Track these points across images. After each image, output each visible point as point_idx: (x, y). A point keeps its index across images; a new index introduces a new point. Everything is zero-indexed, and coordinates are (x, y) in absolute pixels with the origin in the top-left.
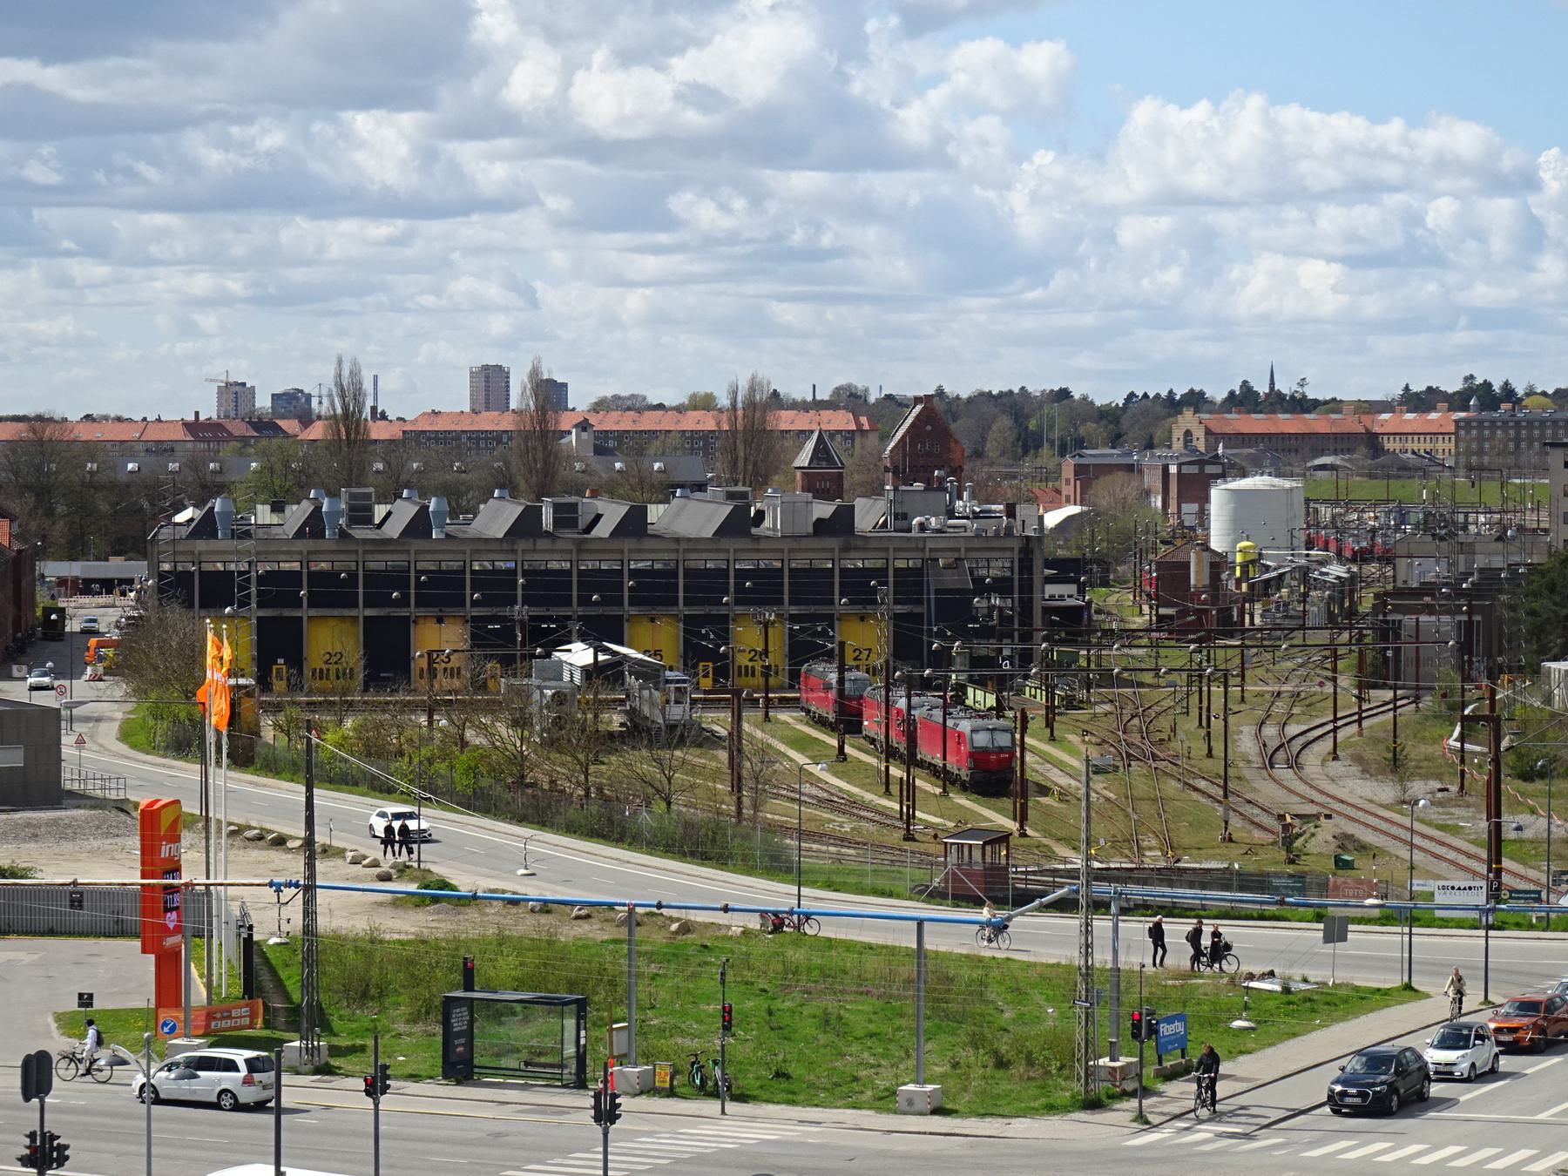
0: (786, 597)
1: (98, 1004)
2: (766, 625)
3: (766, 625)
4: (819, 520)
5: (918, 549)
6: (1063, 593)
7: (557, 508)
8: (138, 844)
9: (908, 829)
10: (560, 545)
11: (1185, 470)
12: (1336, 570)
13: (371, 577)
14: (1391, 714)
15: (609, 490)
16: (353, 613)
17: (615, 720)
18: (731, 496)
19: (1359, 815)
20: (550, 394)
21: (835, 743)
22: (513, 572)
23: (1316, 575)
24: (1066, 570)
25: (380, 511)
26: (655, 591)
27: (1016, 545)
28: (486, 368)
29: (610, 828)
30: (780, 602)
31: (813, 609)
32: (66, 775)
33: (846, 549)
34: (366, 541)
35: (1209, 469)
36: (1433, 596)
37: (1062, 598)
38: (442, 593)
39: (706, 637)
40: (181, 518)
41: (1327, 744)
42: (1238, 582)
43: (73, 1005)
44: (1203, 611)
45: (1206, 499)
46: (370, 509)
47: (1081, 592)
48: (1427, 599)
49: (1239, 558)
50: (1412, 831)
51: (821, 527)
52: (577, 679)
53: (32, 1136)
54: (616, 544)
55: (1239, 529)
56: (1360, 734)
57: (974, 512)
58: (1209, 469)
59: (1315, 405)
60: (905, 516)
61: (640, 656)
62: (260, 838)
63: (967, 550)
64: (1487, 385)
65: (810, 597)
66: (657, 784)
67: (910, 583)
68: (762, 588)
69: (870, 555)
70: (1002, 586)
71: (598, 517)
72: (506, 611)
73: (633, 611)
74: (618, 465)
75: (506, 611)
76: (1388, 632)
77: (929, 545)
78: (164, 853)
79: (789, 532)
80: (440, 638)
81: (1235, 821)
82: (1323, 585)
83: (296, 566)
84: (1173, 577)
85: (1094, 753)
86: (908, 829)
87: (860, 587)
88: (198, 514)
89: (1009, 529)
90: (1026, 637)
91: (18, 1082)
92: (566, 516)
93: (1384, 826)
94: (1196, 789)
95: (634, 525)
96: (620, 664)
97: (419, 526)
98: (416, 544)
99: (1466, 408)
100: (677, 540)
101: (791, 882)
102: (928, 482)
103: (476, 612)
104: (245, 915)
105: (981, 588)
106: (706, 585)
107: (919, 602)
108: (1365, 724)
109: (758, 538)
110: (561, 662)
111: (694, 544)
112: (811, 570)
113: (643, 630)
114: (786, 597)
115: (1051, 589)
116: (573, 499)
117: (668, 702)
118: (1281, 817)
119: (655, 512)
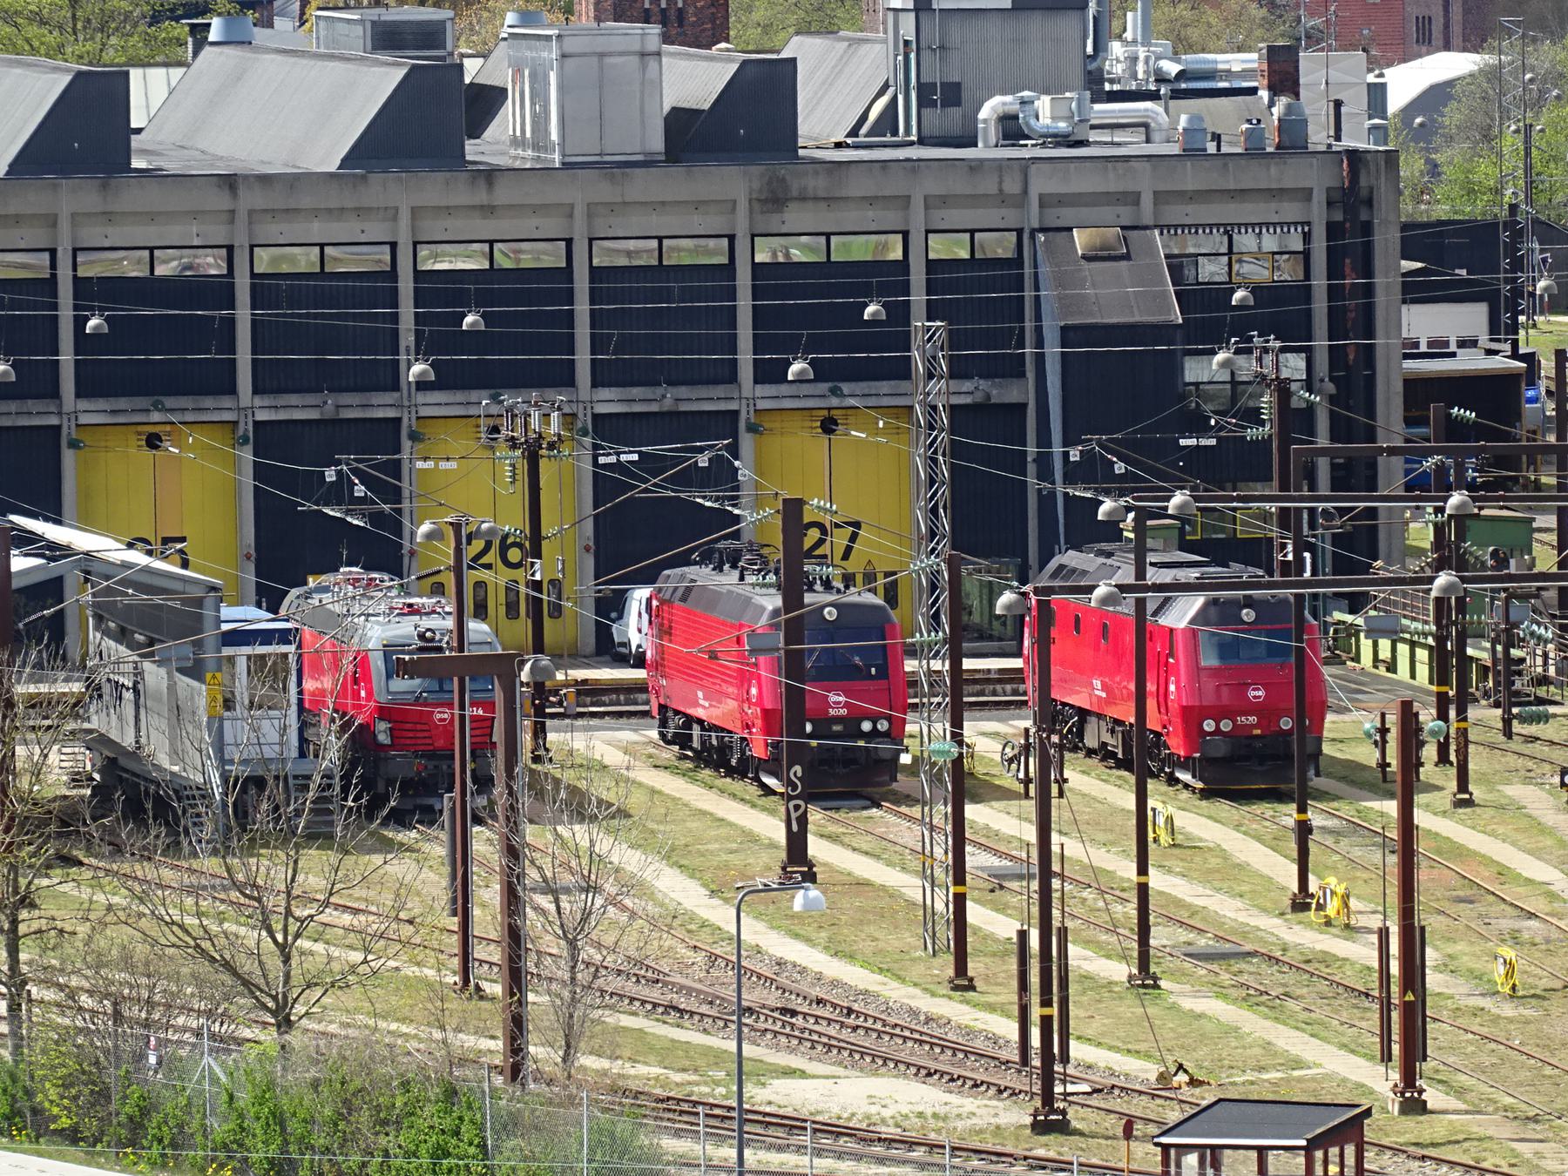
0: (583, 358)
4: (675, 110)
5: (1002, 199)
9: (1048, 1097)
18: (388, 38)
27: (1318, 180)
30: (564, 377)
31: (668, 398)
33: (774, 199)
37: (1439, 349)
39: (339, 494)
51: (690, 136)
57: (1161, 79)
60: (952, 95)
61: (138, 557)
63: (1160, 197)
66: (248, 966)
67: (983, 303)
68: (506, 333)
69: (851, 217)
70: (1279, 312)
73: (92, 412)
77: (1040, 184)
79: (587, 146)
86: (1048, 1097)
87: (832, 325)
90: (1355, 475)
100: (230, 182)
105: (1209, 316)
107: (1014, 368)
109: (490, 175)
114: (583, 358)
115: (1424, 322)
117: (229, 704)
119: (149, 92)
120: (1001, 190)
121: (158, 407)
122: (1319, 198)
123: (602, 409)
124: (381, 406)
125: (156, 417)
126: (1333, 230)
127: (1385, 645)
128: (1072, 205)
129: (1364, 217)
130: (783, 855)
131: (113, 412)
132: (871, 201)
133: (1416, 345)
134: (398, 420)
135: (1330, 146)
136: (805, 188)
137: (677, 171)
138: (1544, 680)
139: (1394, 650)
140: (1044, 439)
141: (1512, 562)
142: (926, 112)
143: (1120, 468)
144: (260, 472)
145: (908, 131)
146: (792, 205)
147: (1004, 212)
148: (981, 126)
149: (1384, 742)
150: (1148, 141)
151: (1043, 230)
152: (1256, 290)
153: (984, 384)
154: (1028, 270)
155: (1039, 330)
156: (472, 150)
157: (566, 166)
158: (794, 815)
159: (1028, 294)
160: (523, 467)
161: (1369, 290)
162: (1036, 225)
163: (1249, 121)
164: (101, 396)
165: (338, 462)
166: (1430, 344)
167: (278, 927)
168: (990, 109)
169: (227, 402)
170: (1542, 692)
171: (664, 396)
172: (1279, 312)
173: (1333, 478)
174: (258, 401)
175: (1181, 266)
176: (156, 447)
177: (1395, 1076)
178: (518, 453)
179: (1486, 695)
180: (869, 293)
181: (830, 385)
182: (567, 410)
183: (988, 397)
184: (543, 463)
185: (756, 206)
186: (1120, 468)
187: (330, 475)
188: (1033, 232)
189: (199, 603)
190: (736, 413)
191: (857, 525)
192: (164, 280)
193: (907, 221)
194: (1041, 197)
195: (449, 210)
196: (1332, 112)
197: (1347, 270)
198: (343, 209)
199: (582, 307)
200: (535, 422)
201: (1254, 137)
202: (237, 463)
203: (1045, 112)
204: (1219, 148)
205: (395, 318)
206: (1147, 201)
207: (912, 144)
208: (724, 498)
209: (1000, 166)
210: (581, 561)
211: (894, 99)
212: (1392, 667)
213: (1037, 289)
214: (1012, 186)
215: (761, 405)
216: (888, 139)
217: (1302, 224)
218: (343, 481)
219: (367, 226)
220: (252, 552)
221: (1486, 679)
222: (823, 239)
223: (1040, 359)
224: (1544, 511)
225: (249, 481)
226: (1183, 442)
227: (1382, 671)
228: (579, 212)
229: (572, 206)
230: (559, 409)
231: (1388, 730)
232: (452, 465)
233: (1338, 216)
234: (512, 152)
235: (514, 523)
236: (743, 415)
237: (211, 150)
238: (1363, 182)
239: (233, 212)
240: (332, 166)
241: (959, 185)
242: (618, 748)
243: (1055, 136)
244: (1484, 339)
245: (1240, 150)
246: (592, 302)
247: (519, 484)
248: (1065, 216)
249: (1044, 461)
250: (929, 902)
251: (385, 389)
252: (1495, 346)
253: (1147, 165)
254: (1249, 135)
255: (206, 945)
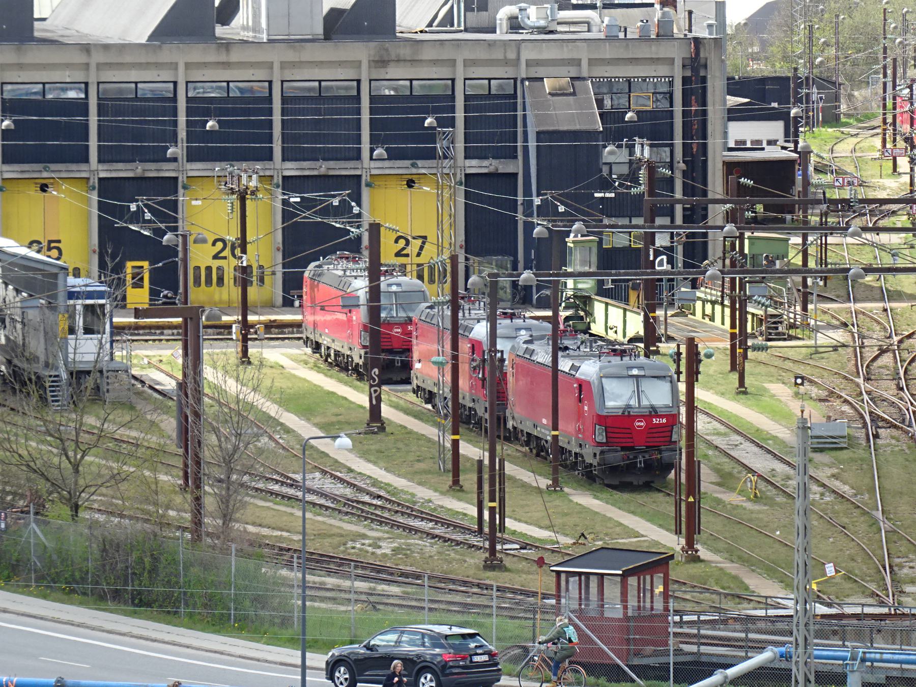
5: (506, 62)
27: (678, 53)
31: (323, 168)
37: (757, 146)
39: (137, 217)
66: (54, 474)
70: (655, 127)
86: (492, 550)
87: (407, 127)
100: (86, 48)
109: (227, 45)
115: (740, 131)
120: (505, 57)
121: (45, 169)
122: (678, 64)
123: (287, 173)
124: (167, 171)
125: (45, 175)
126: (685, 80)
127: (708, 307)
128: (543, 65)
129: (702, 73)
130: (367, 415)
131: (22, 172)
132: (435, 62)
133: (744, 142)
134: (176, 179)
135: (686, 35)
136: (399, 55)
137: (328, 44)
138: (792, 326)
139: (713, 309)
140: (527, 192)
141: (778, 262)
142: (469, 14)
143: (561, 209)
144: (102, 207)
145: (459, 25)
146: (392, 64)
147: (507, 69)
148: (498, 22)
149: (679, 360)
150: (589, 31)
151: (528, 79)
152: (638, 113)
153: (495, 162)
154: (519, 100)
155: (525, 133)
156: (220, 31)
157: (270, 41)
158: (374, 395)
159: (520, 113)
160: (237, 204)
161: (704, 113)
162: (524, 76)
163: (642, 21)
164: (16, 162)
165: (137, 201)
166: (752, 142)
167: (71, 454)
168: (504, 13)
169: (83, 167)
170: (792, 332)
171: (321, 167)
172: (655, 127)
173: (684, 216)
174: (101, 167)
175: (603, 100)
176: (45, 191)
177: (683, 541)
178: (235, 196)
179: (761, 334)
180: (428, 112)
181: (411, 162)
182: (261, 174)
183: (497, 170)
184: (248, 202)
185: (373, 64)
186: (561, 209)
187: (133, 207)
188: (523, 80)
189: (55, 276)
190: (359, 177)
191: (425, 238)
192: (50, 101)
193: (454, 73)
194: (527, 61)
195: (205, 65)
196: (687, 16)
197: (693, 102)
198: (148, 63)
199: (277, 118)
200: (244, 180)
201: (644, 29)
202: (89, 200)
203: (534, 16)
204: (625, 36)
205: (175, 123)
206: (585, 64)
207: (461, 31)
208: (349, 222)
209: (505, 43)
210: (275, 257)
211: (452, 7)
212: (712, 319)
213: (524, 110)
214: (512, 55)
215: (374, 172)
216: (448, 28)
217: (669, 77)
218: (139, 210)
219: (161, 72)
220: (281, 246)
221: (761, 325)
222: (486, 82)
223: (526, 149)
224: (796, 235)
225: (95, 211)
226: (596, 195)
227: (707, 320)
228: (276, 66)
229: (360, 62)
230: (257, 173)
231: (681, 354)
232: (199, 203)
233: (688, 73)
234: (242, 33)
235: (232, 236)
236: (364, 178)
237: (81, 30)
238: (702, 55)
239: (87, 64)
240: (143, 40)
241: (482, 55)
242: (288, 357)
243: (538, 28)
244: (781, 142)
245: (637, 37)
246: (283, 115)
247: (235, 213)
248: (539, 72)
249: (528, 204)
250: (441, 441)
251: (82, 162)
252: (787, 145)
253: (584, 44)
254: (642, 29)
255: (32, 464)
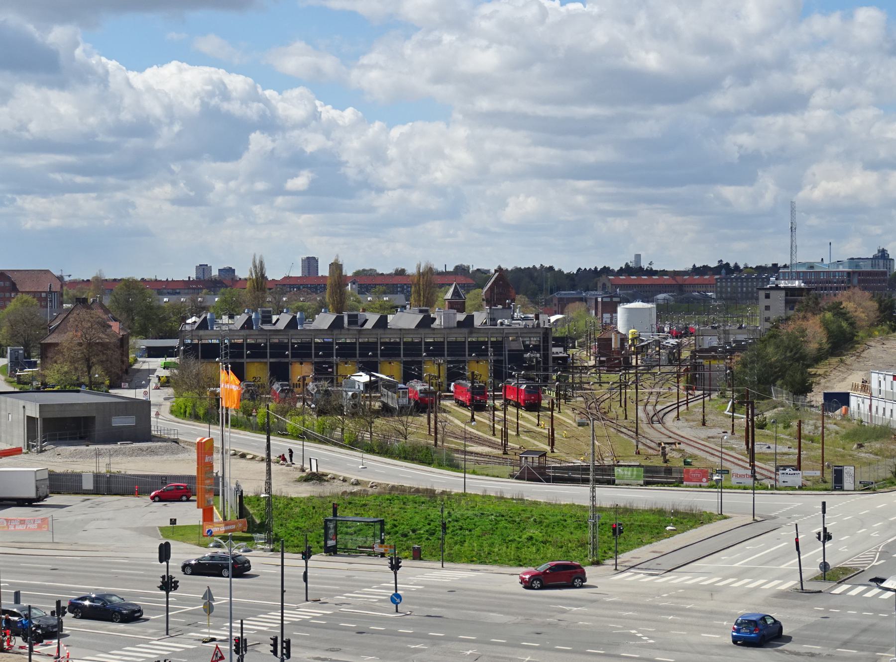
1: (178, 523)
2: (439, 365)
3: (439, 365)
6: (557, 351)
7: (349, 316)
8: (196, 457)
10: (351, 332)
11: (605, 300)
12: (673, 341)
13: (273, 346)
14: (702, 401)
15: (373, 310)
16: (265, 360)
17: (377, 405)
18: (421, 311)
19: (691, 443)
20: (336, 267)
21: (470, 414)
22: (332, 343)
23: (664, 343)
24: (562, 342)
25: (275, 318)
26: (391, 351)
28: (308, 258)
29: (383, 450)
32: (152, 428)
33: (471, 333)
34: (270, 330)
35: (615, 299)
36: (716, 352)
37: (557, 353)
38: (303, 352)
39: (414, 370)
40: (189, 321)
41: (675, 413)
42: (630, 346)
43: (167, 523)
44: (614, 357)
45: (616, 312)
46: (270, 317)
47: (565, 351)
48: (713, 353)
49: (630, 337)
50: (722, 452)
52: (362, 388)
53: (163, 577)
54: (375, 332)
55: (630, 324)
56: (688, 409)
58: (615, 299)
59: (655, 273)
62: (235, 455)
64: (728, 264)
65: (456, 352)
67: (498, 346)
68: (436, 350)
70: (536, 348)
71: (367, 320)
72: (330, 360)
73: (382, 359)
74: (369, 299)
75: (330, 360)
76: (696, 367)
77: (506, 331)
78: (207, 460)
79: (447, 325)
80: (301, 371)
81: (640, 446)
82: (664, 347)
83: (241, 341)
84: (604, 345)
85: (578, 418)
87: (478, 349)
88: (199, 320)
89: (538, 324)
91: (157, 555)
92: (353, 320)
93: (703, 447)
94: (622, 432)
95: (382, 323)
96: (376, 382)
97: (293, 324)
98: (292, 332)
99: (720, 274)
101: (606, 504)
102: (504, 304)
103: (316, 360)
104: (238, 486)
105: (527, 349)
106: (413, 349)
107: (501, 355)
108: (690, 405)
109: (434, 329)
110: (355, 381)
111: (408, 331)
112: (456, 342)
113: (386, 367)
115: (555, 350)
116: (355, 313)
118: (660, 444)
119: (390, 318)
